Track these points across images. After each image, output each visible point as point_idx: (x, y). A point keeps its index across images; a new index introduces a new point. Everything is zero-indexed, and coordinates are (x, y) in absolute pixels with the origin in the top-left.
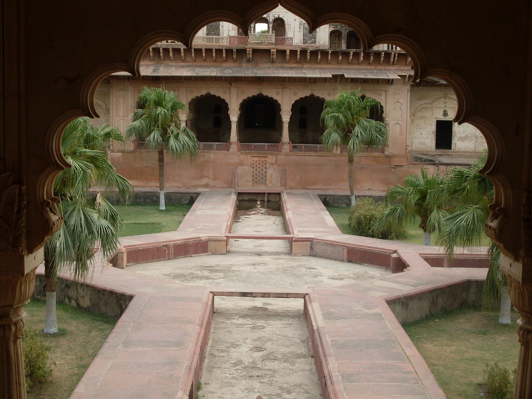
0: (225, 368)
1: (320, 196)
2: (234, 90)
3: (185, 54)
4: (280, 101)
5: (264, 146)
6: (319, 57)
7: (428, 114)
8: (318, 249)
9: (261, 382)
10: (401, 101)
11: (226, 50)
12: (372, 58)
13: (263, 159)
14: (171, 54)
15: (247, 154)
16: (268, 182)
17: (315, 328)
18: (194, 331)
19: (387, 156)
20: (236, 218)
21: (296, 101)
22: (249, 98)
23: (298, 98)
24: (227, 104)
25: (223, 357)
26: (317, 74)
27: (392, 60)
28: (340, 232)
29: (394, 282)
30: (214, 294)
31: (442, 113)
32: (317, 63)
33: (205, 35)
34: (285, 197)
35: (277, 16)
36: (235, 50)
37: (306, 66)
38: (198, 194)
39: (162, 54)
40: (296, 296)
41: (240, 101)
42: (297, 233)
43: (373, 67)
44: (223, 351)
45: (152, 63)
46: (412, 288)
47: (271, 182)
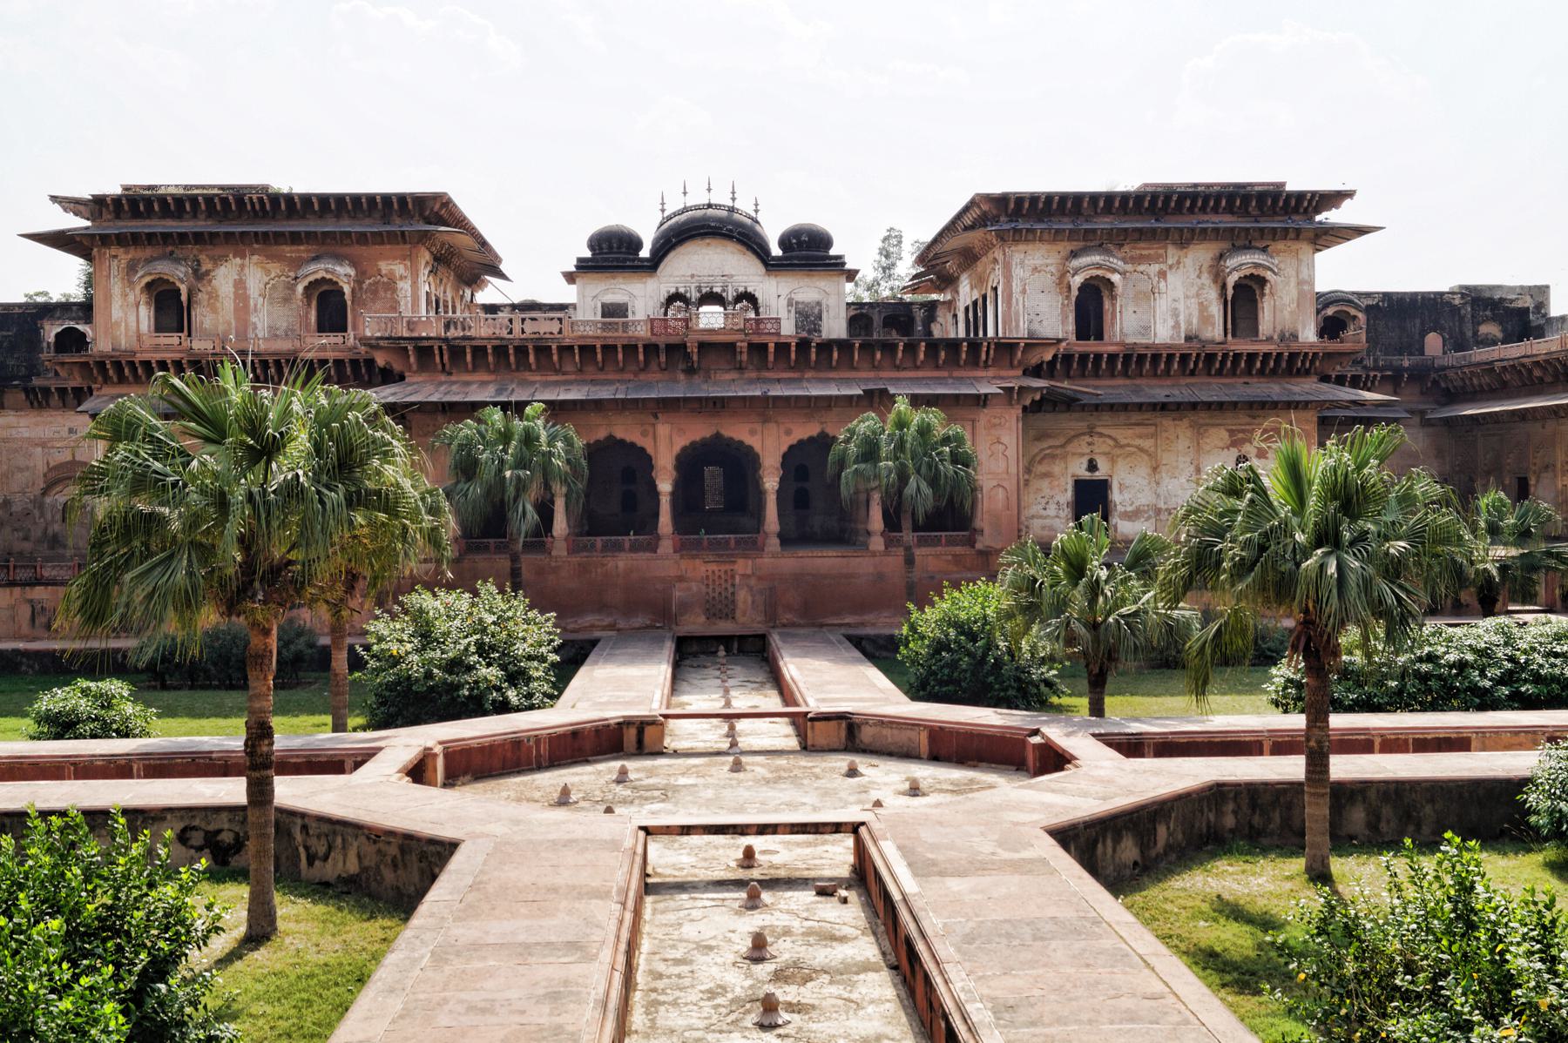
0: (686, 1004)
1: (849, 638)
2: (663, 429)
3: (560, 358)
4: (757, 447)
5: (727, 541)
6: (835, 355)
7: (1057, 468)
8: (866, 735)
9: (779, 1036)
10: (1005, 439)
11: (645, 346)
12: (943, 354)
13: (728, 567)
14: (532, 358)
15: (693, 557)
16: (738, 614)
17: (896, 896)
18: (608, 916)
19: (980, 553)
20: (674, 690)
21: (791, 447)
22: (693, 443)
23: (793, 439)
24: (650, 458)
25: (679, 976)
26: (833, 391)
27: (983, 357)
28: (905, 699)
29: (1053, 791)
30: (647, 831)
31: (1085, 465)
32: (831, 368)
33: (599, 318)
34: (775, 639)
35: (741, 289)
36: (662, 346)
37: (809, 375)
38: (594, 643)
39: (512, 358)
40: (837, 828)
41: (677, 449)
42: (814, 703)
43: (945, 374)
44: (677, 962)
45: (492, 377)
46: (1098, 802)
47: (744, 614)
